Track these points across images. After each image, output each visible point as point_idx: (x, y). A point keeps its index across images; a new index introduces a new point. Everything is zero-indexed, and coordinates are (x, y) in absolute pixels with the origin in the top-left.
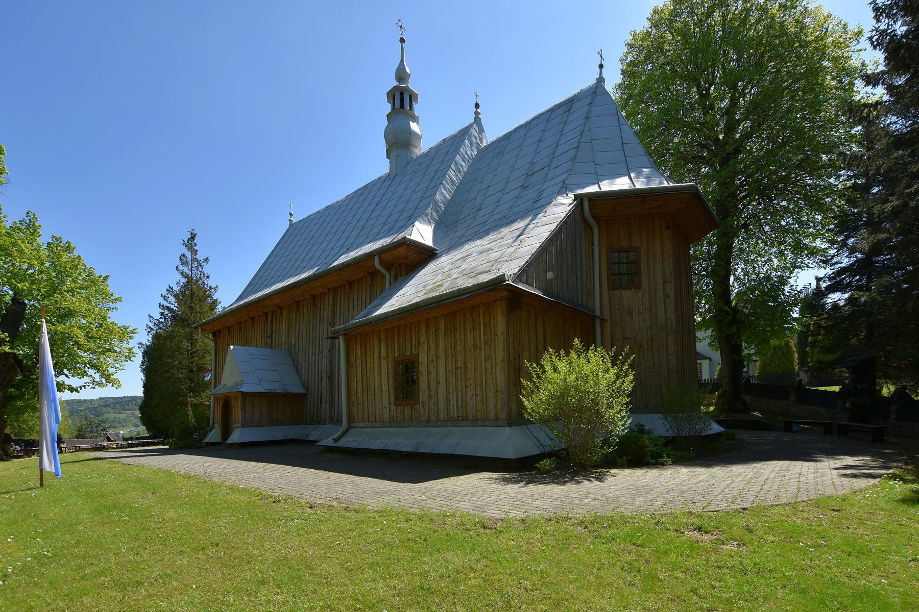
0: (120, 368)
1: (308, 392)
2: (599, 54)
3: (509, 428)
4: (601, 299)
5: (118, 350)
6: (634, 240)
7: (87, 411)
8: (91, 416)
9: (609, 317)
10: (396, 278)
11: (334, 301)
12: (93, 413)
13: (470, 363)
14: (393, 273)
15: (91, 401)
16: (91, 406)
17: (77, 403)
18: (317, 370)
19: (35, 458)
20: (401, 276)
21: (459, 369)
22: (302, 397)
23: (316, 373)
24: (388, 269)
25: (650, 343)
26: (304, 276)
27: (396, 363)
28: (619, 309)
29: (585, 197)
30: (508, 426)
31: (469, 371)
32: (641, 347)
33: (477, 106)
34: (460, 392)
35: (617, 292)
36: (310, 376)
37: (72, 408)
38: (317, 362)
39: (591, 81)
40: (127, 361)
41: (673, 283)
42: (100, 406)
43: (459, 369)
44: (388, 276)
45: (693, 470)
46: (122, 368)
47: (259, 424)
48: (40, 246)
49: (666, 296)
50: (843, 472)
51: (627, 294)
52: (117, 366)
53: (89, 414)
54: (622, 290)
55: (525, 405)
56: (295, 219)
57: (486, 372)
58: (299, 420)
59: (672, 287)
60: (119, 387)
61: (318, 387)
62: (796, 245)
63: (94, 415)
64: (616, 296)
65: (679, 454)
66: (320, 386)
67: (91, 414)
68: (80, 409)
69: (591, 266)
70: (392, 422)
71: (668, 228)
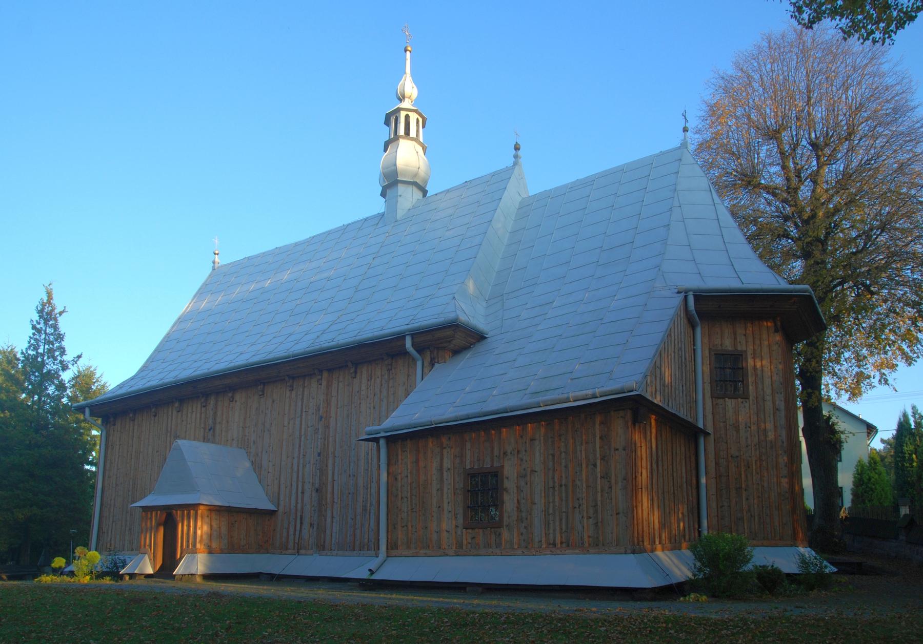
1: (278, 509)
2: (683, 115)
3: (632, 555)
4: (704, 409)
6: (740, 342)
9: (712, 430)
10: (432, 365)
11: (329, 386)
13: (579, 480)
14: (428, 359)
18: (295, 479)
20: (438, 363)
21: (564, 487)
22: (272, 513)
23: (294, 484)
24: (420, 350)
25: (758, 463)
27: (471, 475)
28: (724, 422)
30: (631, 553)
31: (578, 490)
32: (749, 467)
33: (517, 148)
34: (564, 514)
35: (721, 401)
36: (282, 487)
38: (295, 469)
39: (677, 143)
41: (783, 395)
43: (564, 487)
44: (419, 364)
45: (822, 615)
47: (243, 550)
48: (871, 472)
49: (776, 410)
51: (730, 403)
54: (727, 399)
56: (220, 260)
57: (602, 491)
58: (264, 547)
59: (783, 399)
61: (297, 503)
64: (721, 406)
66: (300, 501)
69: (693, 370)
70: (460, 550)
71: (776, 331)
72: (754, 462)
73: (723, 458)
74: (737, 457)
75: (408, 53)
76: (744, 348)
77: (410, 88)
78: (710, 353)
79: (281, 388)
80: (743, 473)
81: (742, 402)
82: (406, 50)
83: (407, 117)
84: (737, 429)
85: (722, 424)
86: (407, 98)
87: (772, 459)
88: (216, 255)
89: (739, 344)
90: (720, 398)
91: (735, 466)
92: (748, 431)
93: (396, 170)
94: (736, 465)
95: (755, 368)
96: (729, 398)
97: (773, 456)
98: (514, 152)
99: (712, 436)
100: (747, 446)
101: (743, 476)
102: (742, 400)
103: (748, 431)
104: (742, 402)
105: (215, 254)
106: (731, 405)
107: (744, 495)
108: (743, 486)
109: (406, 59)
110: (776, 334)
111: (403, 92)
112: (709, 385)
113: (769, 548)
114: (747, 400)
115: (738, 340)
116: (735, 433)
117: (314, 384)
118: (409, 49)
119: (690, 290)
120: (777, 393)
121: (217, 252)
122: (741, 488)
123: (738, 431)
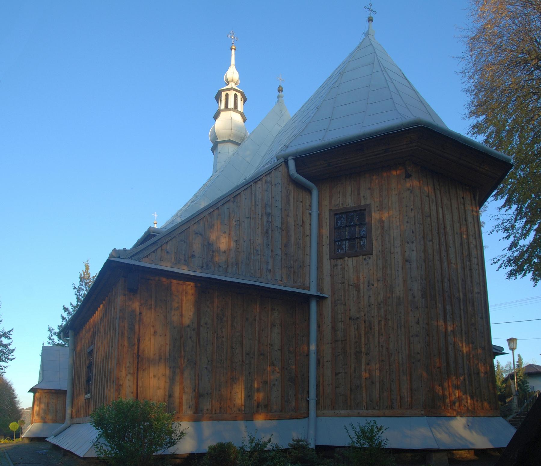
32: (371, 329)
33: (280, 90)
35: (339, 262)
51: (350, 262)
54: (346, 258)
72: (376, 323)
73: (341, 322)
74: (358, 318)
75: (233, 51)
76: (368, 202)
77: (232, 74)
78: (330, 213)
79: (273, 310)
80: (363, 335)
81: (365, 259)
82: (231, 49)
83: (227, 95)
84: (357, 287)
85: (341, 286)
86: (231, 82)
87: (400, 317)
88: (155, 224)
89: (362, 198)
90: (340, 258)
91: (355, 328)
92: (371, 289)
93: (216, 135)
94: (356, 327)
95: (381, 221)
96: (349, 257)
97: (400, 313)
98: (277, 93)
99: (329, 302)
100: (369, 306)
101: (363, 339)
102: (364, 257)
103: (371, 289)
104: (365, 259)
105: (154, 224)
106: (353, 263)
107: (363, 360)
108: (363, 350)
109: (231, 55)
110: (407, 180)
111: (226, 79)
112: (328, 246)
113: (393, 418)
114: (371, 256)
115: (362, 195)
116: (355, 293)
117: (75, 303)
118: (233, 47)
119: (289, 156)
120: (408, 243)
121: (155, 222)
122: (360, 352)
123: (358, 291)
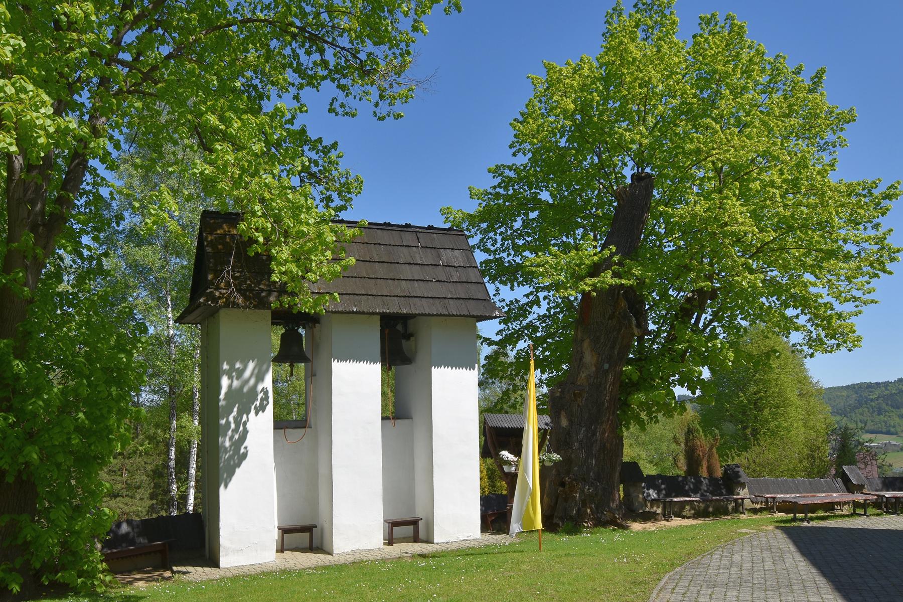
0: (864, 298)
5: (852, 248)
7: (881, 400)
8: (886, 408)
12: (890, 403)
15: (886, 384)
16: (887, 392)
17: (867, 388)
19: (880, 486)
26: (304, 343)
29: (311, 375)
37: (861, 396)
40: (876, 275)
42: (899, 393)
46: (868, 297)
50: (777, 524)
52: (858, 294)
53: (884, 405)
55: (643, 222)
60: (855, 346)
62: (85, 43)
63: (892, 407)
65: (636, 331)
67: (887, 404)
68: (871, 397)
